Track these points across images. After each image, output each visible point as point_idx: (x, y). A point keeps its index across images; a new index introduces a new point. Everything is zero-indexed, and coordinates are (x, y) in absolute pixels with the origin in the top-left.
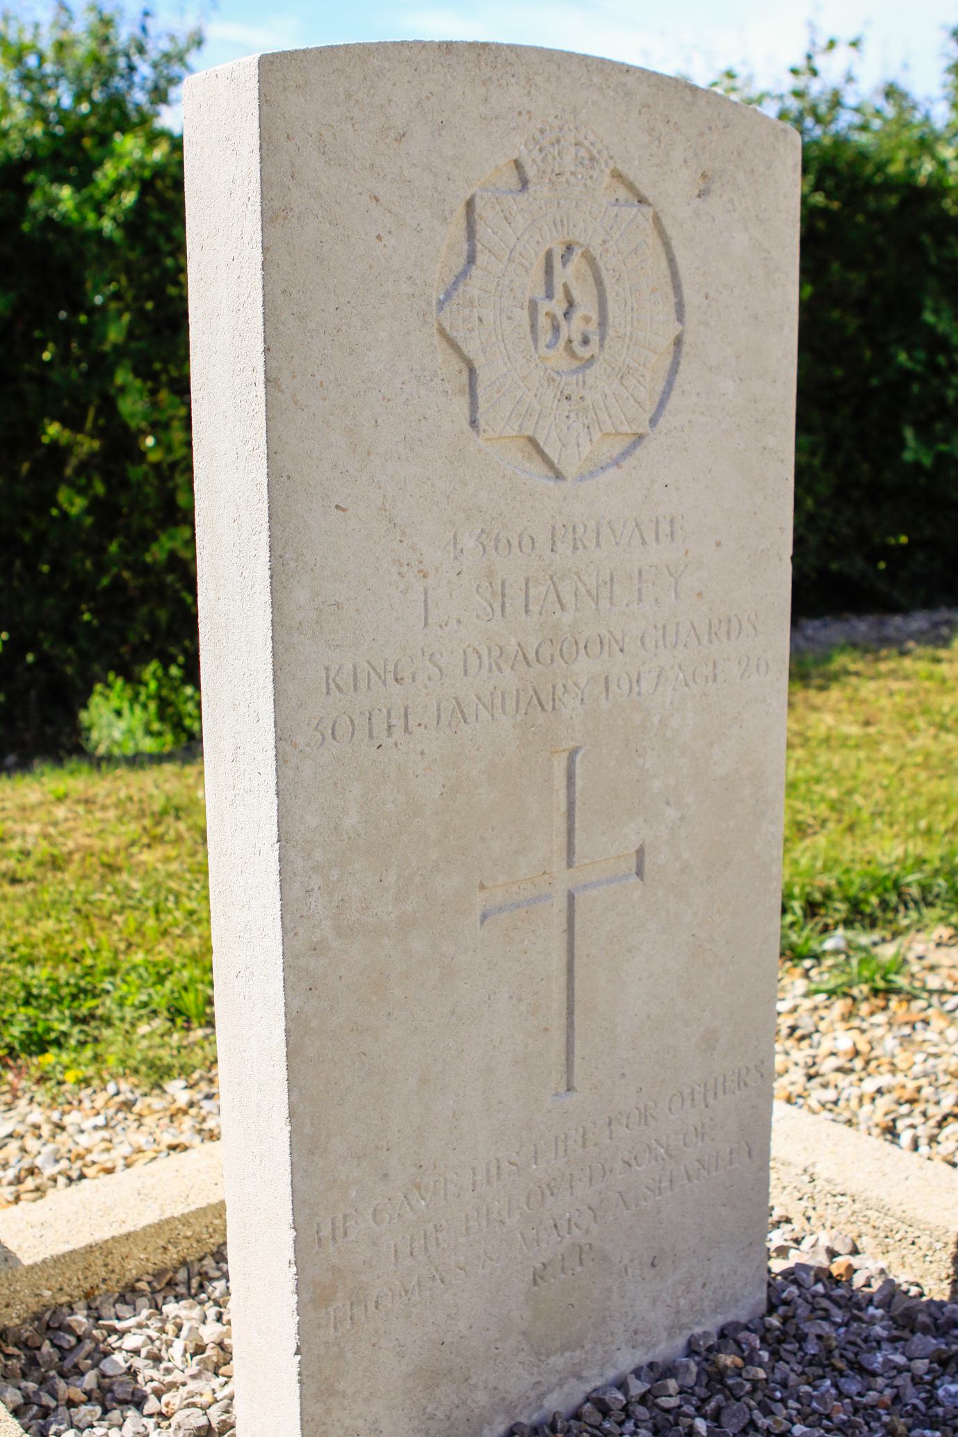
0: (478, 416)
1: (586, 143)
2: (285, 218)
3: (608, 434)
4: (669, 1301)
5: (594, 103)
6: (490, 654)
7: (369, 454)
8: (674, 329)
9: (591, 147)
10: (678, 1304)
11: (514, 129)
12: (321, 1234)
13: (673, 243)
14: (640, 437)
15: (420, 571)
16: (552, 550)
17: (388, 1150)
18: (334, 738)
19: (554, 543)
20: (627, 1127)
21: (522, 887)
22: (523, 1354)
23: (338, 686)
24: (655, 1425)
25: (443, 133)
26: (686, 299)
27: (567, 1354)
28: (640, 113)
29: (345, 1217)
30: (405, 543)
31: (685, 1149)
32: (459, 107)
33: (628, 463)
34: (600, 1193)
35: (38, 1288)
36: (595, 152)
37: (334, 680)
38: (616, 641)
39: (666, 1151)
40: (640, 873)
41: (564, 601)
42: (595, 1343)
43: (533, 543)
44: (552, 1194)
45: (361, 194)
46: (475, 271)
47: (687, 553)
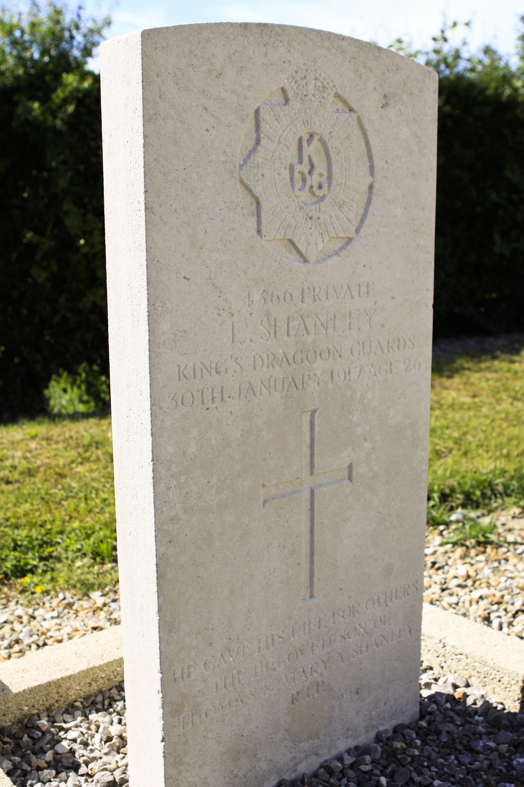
0: (262, 228)
3: (333, 238)
6: (268, 358)
7: (202, 248)
9: (323, 81)
11: (281, 71)
16: (302, 301)
17: (212, 630)
19: (303, 297)
20: (343, 617)
23: (185, 376)
25: (242, 73)
26: (375, 164)
27: (310, 742)
28: (350, 62)
29: (189, 666)
30: (222, 297)
31: (375, 629)
32: (251, 59)
33: (343, 254)
34: (328, 653)
36: (325, 83)
37: (183, 372)
39: (365, 630)
42: (326, 735)
44: (302, 654)
45: (197, 106)
46: (259, 148)
47: (376, 303)
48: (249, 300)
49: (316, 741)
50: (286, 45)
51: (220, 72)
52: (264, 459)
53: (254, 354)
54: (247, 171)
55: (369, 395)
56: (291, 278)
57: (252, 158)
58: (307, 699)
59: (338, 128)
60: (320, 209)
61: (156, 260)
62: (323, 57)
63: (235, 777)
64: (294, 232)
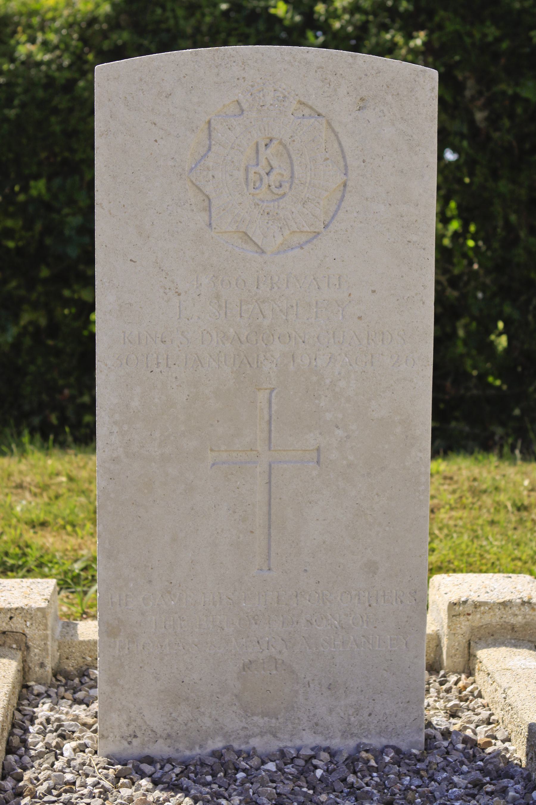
0: (212, 222)
1: (280, 89)
2: (107, 135)
3: (294, 232)
4: (342, 714)
5: (285, 70)
6: (217, 335)
7: (149, 237)
8: (340, 179)
10: (349, 719)
11: (235, 86)
12: (113, 600)
13: (339, 135)
14: (318, 233)
15: (176, 292)
16: (257, 288)
17: (152, 569)
18: (127, 364)
19: (258, 285)
20: (309, 601)
21: (239, 455)
22: (235, 708)
23: (130, 341)
24: (303, 770)
26: (348, 162)
27: (266, 719)
28: (316, 72)
29: (127, 595)
32: (202, 79)
35: (84, 654)
36: (286, 94)
37: (128, 338)
38: (300, 337)
39: (339, 623)
40: (318, 462)
41: (264, 314)
42: (287, 720)
43: (245, 283)
44: (256, 624)
45: (146, 122)
46: (210, 154)
47: (350, 295)
48: (197, 283)
49: (274, 721)
50: (241, 64)
51: (169, 93)
52: (212, 425)
53: (201, 330)
54: (196, 173)
55: (342, 384)
56: (244, 267)
57: (202, 163)
58: (263, 672)
59: (301, 132)
60: (279, 206)
61: (104, 245)
62: (283, 70)
63: (174, 720)
64: (248, 225)
